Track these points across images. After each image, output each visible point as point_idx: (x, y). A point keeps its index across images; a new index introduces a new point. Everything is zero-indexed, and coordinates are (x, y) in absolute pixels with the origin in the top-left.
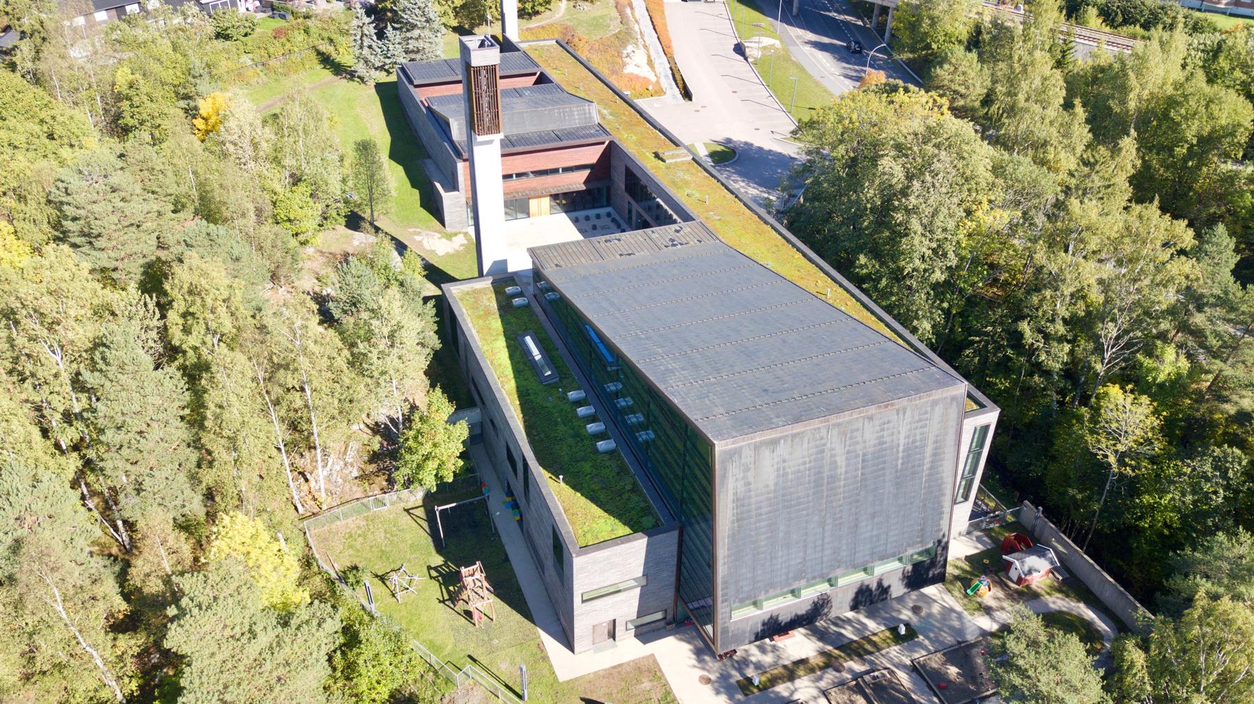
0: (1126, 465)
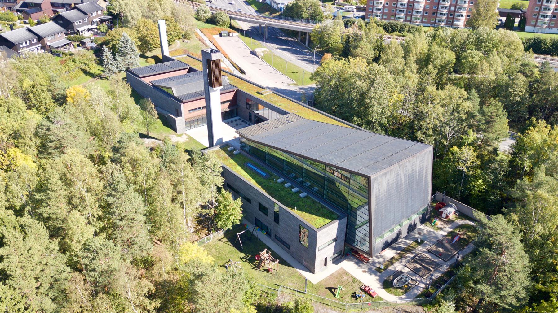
0: (470, 171)
